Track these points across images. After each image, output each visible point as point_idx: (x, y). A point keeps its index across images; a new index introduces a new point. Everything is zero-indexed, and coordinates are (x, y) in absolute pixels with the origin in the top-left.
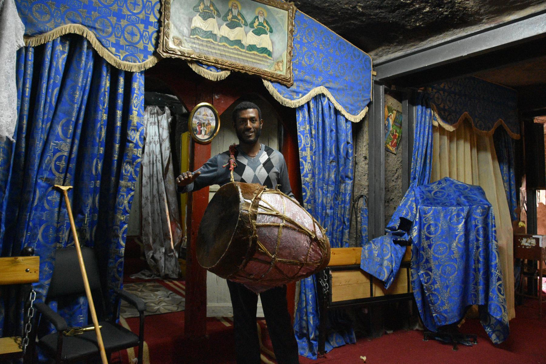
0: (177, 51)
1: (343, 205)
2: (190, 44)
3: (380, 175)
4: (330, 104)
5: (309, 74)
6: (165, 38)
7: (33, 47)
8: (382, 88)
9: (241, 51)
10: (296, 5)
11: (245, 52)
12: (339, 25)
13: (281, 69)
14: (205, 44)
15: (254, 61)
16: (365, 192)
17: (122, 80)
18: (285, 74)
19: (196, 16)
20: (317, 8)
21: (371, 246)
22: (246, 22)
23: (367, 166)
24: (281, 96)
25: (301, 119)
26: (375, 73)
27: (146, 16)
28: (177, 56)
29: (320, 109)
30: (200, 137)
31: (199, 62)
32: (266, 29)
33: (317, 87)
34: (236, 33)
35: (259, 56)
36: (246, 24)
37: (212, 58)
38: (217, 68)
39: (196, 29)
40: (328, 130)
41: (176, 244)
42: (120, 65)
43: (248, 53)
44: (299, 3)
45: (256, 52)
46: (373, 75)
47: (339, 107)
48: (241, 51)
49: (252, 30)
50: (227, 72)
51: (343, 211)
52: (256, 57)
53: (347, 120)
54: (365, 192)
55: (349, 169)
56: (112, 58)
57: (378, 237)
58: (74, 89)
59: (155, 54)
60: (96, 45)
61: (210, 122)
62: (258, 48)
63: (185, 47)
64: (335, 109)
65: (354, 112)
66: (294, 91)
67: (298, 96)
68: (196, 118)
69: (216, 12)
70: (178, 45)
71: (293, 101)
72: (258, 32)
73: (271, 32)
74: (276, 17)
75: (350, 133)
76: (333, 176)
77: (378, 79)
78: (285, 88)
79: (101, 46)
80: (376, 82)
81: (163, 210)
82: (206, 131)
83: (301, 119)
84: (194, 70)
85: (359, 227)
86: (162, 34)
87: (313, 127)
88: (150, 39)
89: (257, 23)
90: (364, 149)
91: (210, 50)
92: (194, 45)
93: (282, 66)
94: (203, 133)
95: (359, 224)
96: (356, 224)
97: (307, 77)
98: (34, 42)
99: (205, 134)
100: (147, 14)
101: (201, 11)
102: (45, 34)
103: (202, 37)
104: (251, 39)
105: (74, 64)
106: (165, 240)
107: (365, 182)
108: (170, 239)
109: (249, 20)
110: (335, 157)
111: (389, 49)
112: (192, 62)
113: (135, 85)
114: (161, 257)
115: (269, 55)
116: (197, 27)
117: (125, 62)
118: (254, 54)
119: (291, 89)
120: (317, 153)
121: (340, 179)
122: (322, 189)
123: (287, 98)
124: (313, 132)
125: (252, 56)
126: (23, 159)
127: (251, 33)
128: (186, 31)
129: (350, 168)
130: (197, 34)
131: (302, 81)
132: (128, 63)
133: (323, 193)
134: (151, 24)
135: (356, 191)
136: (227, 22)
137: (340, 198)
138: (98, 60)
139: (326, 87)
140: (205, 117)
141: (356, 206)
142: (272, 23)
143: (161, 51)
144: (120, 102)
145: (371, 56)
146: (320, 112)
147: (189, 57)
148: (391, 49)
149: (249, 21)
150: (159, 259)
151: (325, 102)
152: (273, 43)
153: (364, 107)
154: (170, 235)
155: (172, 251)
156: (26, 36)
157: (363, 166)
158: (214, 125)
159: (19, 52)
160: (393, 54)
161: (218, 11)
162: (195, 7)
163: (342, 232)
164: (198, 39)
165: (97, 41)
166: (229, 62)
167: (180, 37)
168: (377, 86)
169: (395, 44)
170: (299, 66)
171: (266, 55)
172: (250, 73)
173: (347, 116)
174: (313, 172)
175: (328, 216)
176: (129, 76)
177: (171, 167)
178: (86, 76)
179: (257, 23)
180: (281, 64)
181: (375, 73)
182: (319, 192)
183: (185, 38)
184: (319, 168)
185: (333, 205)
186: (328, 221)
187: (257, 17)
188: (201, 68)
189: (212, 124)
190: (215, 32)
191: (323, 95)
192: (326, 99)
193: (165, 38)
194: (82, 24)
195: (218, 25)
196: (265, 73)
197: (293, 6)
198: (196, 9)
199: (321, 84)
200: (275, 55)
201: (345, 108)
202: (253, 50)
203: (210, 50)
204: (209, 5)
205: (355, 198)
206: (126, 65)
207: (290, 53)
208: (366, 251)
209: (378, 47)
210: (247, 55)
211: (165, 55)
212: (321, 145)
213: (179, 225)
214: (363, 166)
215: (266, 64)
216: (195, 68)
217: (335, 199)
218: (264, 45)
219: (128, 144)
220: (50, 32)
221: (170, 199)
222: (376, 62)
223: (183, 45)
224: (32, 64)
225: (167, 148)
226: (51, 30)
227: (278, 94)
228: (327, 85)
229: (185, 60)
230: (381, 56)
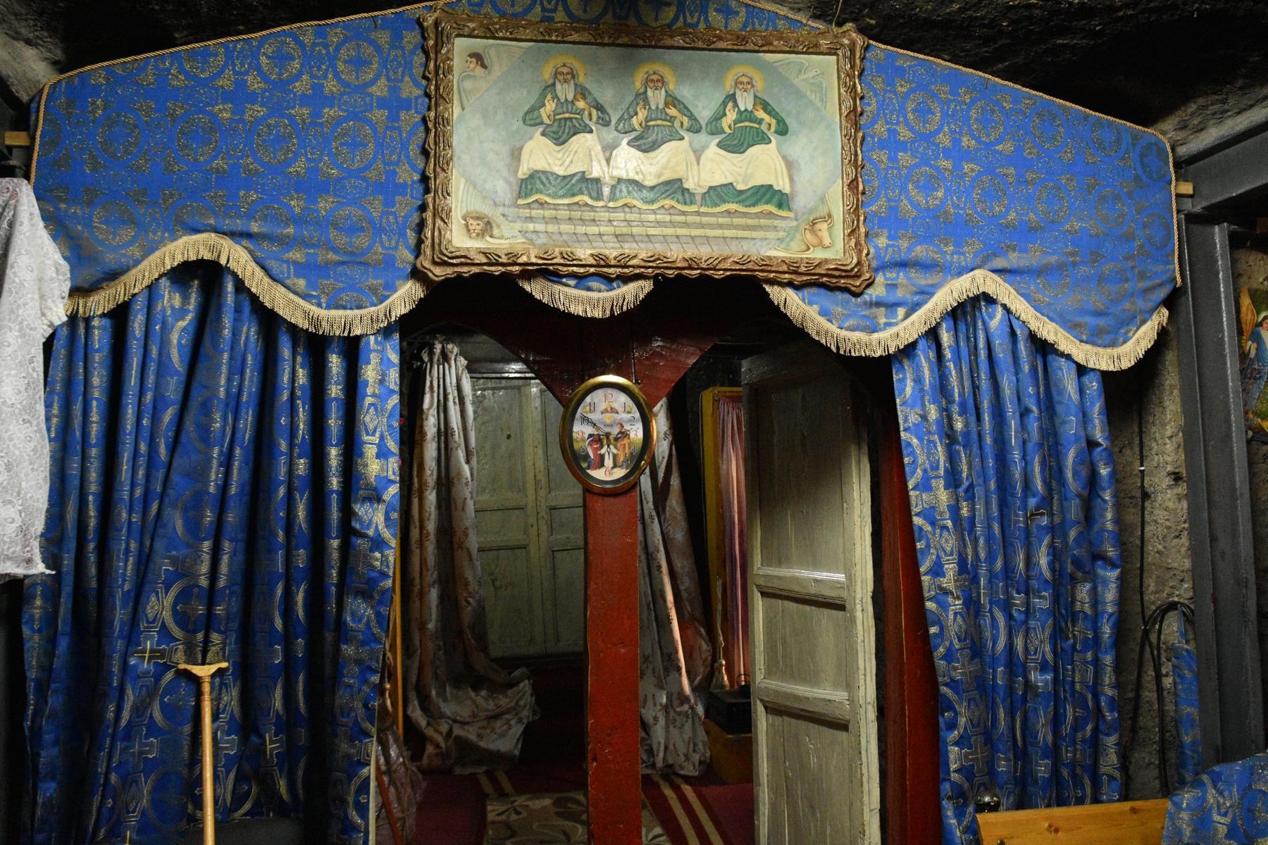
0: (472, 255)
1: (1089, 656)
2: (518, 226)
3: (1234, 535)
4: (1015, 323)
5: (926, 239)
6: (439, 222)
7: (103, 315)
8: (1219, 235)
9: (684, 213)
10: (862, 31)
11: (698, 213)
12: (1020, 60)
13: (827, 241)
14: (563, 214)
15: (728, 233)
16: (1183, 593)
17: (335, 362)
18: (840, 255)
19: (531, 138)
20: (929, 23)
21: (1204, 799)
22: (692, 117)
23: (1185, 504)
24: (833, 328)
25: (909, 390)
26: (1187, 188)
27: (386, 172)
28: (475, 270)
29: (982, 344)
30: (599, 474)
31: (548, 273)
32: (764, 127)
33: (960, 274)
34: (664, 161)
35: (745, 215)
36: (695, 129)
37: (584, 253)
38: (608, 280)
39: (534, 176)
40: (1010, 410)
41: (696, 682)
42: (316, 322)
43: (707, 214)
44: (873, 22)
45: (733, 207)
46: (1178, 196)
47: (1049, 331)
48: (684, 213)
49: (717, 139)
50: (641, 283)
51: (1090, 675)
52: (736, 221)
53: (1082, 370)
54: (1183, 593)
55: (1103, 530)
56: (297, 306)
57: (1235, 760)
58: (206, 409)
59: (417, 274)
60: (257, 281)
61: (627, 427)
62: (741, 192)
63: (501, 238)
64: (1033, 337)
65: (1107, 338)
66: (878, 304)
67: (895, 315)
68: (585, 420)
69: (594, 112)
70: (481, 235)
71: (875, 335)
72: (736, 144)
73: (783, 130)
74: (796, 81)
75: (1096, 409)
76: (1043, 561)
77: (1198, 209)
78: (847, 296)
79: (267, 280)
80: (1191, 219)
81: (658, 595)
82: (615, 456)
83: (909, 390)
84: (538, 296)
85: (1170, 707)
86: (429, 215)
87: (955, 408)
88: (402, 234)
89: (731, 116)
90: (1170, 447)
91: (581, 229)
92: (531, 226)
93: (830, 229)
94: (609, 462)
95: (1168, 698)
96: (1160, 699)
97: (920, 251)
98: (100, 303)
99: (615, 466)
100: (390, 163)
101: (546, 121)
102: (124, 278)
103: (554, 196)
104: (715, 167)
105: (207, 343)
106: (667, 670)
107: (1180, 560)
108: (679, 669)
109: (704, 113)
110: (1043, 498)
111: (1224, 102)
112: (531, 273)
113: (370, 373)
114: (656, 719)
115: (780, 206)
116: (537, 171)
117: (334, 313)
118: (728, 213)
119: (866, 297)
120: (979, 491)
121: (1070, 568)
122: (1007, 607)
123: (852, 329)
124: (959, 426)
125: (721, 220)
126: (92, 608)
127: (713, 151)
128: (502, 188)
129: (1109, 526)
130: (539, 191)
131: (903, 265)
132: (341, 312)
133: (1010, 617)
134: (401, 189)
135: (1152, 588)
136: (634, 135)
137: (1080, 630)
138: (268, 320)
139: (993, 271)
140: (608, 418)
141: (1153, 637)
142: (784, 106)
143: (427, 264)
144: (334, 422)
145: (1164, 133)
146: (983, 354)
147: (515, 264)
148: (1231, 102)
149: (704, 115)
150: (651, 721)
151: (996, 321)
152: (790, 165)
153: (1151, 312)
154: (678, 660)
155: (684, 699)
156: (77, 291)
157: (1168, 506)
158: (640, 435)
159: (48, 346)
160: (1240, 119)
161: (600, 108)
162: (527, 113)
163: (1095, 744)
164: (542, 204)
165: (258, 269)
166: (643, 255)
167: (486, 210)
168: (1197, 229)
169: (1240, 83)
170: (893, 222)
171: (771, 208)
172: (719, 275)
173: (1082, 352)
174: (960, 555)
175: (1037, 695)
176: (352, 348)
177: (675, 481)
178: (238, 368)
179: (731, 116)
180: (824, 226)
181: (1187, 188)
182: (993, 619)
183: (501, 209)
184: (989, 538)
185: (1049, 657)
186: (1036, 710)
187: (732, 97)
188: (557, 288)
189: (632, 435)
190: (595, 173)
191: (989, 299)
192: (1000, 309)
193: (439, 222)
194: (216, 231)
195: (604, 149)
196: (766, 265)
197: (851, 35)
198: (531, 118)
199: (978, 260)
200: (802, 201)
201: (1072, 327)
202: (724, 202)
203: (581, 229)
204: (570, 97)
205: (1148, 613)
206: (334, 320)
207: (853, 185)
208: (1185, 816)
209: (1185, 100)
210: (705, 220)
211: (439, 273)
212: (991, 462)
213: (703, 630)
214: (1171, 505)
215: (771, 235)
216: (537, 289)
217: (1058, 635)
218: (761, 178)
219: (353, 539)
220: (134, 271)
221: (678, 564)
222: (1183, 151)
223: (496, 232)
224: (87, 367)
225: (662, 435)
226: (137, 262)
227: (822, 321)
228: (999, 263)
229: (503, 274)
230: (1200, 129)
